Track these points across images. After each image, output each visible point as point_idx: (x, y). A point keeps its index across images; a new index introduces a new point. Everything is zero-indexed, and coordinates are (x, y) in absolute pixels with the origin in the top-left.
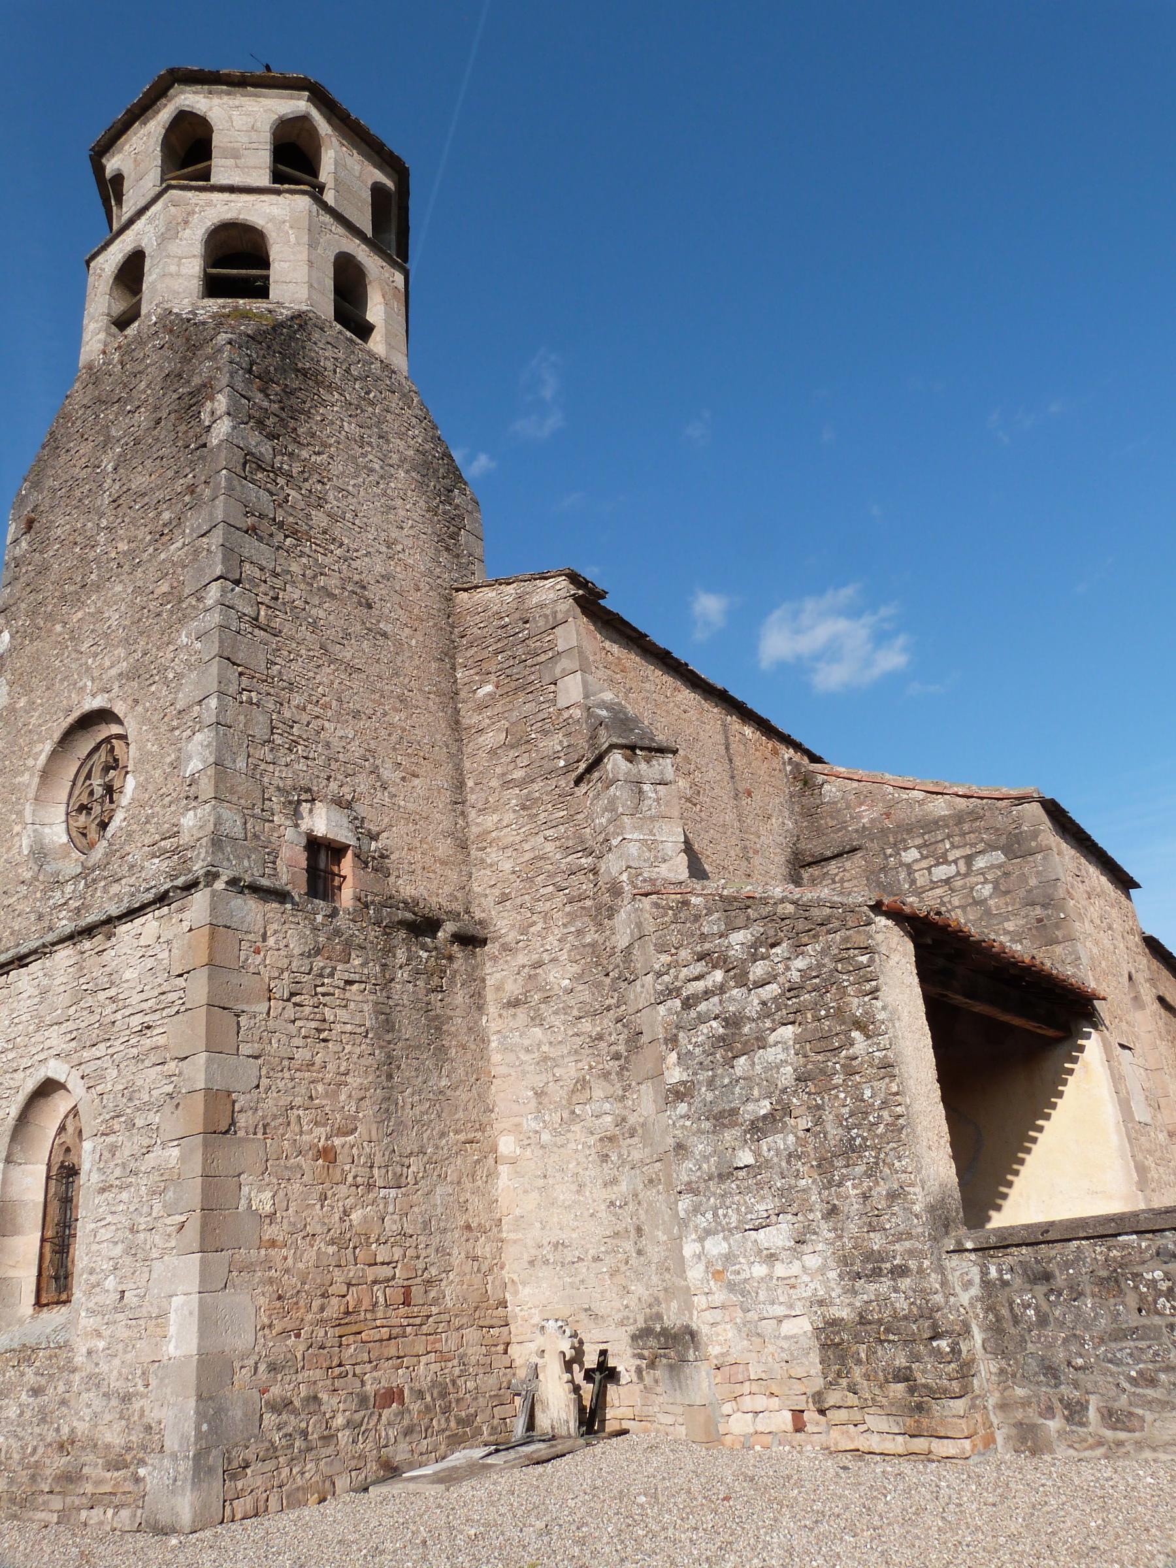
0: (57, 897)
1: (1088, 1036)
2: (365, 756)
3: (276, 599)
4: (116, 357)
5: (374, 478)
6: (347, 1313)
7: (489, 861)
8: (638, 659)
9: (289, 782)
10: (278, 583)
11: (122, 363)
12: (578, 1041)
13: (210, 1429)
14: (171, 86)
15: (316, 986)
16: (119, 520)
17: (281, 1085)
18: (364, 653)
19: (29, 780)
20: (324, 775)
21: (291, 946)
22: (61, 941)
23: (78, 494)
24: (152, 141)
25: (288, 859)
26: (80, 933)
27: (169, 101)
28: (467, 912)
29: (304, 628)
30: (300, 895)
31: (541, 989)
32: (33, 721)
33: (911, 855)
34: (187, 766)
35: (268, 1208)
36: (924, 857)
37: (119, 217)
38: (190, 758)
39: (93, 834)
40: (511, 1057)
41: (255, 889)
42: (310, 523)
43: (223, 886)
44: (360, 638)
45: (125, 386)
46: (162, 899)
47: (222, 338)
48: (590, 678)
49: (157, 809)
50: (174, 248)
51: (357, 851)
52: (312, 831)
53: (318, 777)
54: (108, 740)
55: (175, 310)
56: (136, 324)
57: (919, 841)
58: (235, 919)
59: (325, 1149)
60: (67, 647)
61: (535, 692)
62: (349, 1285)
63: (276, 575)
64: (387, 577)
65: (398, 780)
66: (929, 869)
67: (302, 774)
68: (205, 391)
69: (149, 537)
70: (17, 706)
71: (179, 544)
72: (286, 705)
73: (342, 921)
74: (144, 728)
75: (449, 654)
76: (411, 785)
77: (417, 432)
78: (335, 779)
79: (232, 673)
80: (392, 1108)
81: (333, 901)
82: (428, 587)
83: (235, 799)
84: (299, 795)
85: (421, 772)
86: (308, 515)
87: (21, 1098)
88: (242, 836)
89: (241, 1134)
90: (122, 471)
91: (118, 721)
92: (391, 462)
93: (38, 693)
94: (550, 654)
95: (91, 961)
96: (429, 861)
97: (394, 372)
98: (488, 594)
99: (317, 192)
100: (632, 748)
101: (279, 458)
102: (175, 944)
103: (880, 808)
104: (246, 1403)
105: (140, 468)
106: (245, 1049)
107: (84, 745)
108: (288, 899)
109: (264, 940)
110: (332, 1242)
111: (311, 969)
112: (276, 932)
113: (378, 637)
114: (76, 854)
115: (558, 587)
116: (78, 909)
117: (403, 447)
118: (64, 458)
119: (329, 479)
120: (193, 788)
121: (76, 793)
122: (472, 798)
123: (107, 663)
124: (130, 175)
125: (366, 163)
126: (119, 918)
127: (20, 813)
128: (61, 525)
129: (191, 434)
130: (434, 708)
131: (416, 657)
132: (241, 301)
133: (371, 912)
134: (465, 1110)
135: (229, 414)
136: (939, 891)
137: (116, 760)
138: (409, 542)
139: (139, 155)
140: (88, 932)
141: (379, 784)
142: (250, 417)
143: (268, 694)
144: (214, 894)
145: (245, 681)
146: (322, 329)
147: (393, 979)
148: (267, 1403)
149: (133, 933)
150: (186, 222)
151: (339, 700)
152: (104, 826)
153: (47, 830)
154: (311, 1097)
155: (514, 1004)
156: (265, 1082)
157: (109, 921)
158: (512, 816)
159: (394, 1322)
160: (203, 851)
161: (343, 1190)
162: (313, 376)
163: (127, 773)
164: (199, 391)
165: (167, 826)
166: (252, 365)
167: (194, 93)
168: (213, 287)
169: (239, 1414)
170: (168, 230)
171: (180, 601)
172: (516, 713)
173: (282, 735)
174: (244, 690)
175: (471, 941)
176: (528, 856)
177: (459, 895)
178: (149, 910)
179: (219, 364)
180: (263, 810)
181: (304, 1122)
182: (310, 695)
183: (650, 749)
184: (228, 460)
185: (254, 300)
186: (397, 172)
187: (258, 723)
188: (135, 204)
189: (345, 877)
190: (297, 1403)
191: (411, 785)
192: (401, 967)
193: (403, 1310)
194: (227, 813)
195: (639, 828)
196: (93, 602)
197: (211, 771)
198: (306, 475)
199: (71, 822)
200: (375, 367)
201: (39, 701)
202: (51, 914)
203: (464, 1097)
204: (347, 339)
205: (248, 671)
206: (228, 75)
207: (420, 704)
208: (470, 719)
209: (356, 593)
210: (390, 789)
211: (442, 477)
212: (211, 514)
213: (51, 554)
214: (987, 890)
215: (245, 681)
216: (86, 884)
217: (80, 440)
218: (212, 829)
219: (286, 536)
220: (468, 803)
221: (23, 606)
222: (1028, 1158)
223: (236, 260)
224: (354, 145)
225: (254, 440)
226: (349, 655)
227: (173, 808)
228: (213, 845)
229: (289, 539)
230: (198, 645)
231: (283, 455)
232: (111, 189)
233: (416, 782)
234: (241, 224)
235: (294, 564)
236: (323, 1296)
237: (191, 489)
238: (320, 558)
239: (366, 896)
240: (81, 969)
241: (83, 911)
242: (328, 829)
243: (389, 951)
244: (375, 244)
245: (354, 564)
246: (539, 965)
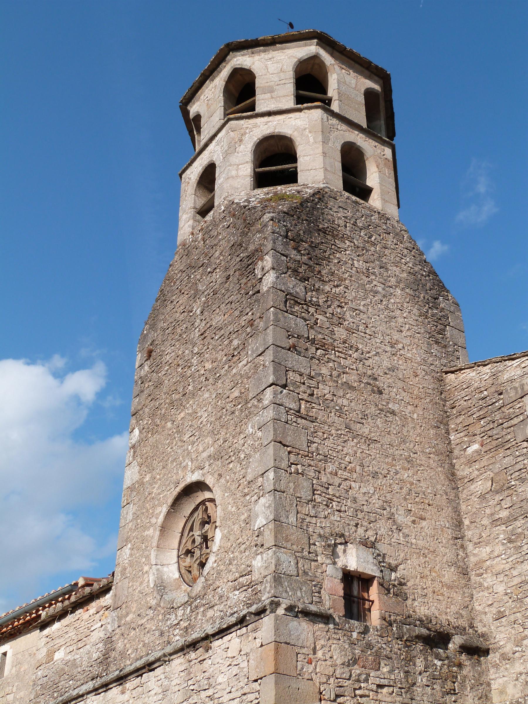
0: (173, 619)
2: (383, 506)
3: (312, 395)
4: (200, 236)
5: (378, 297)
7: (486, 585)
9: (328, 530)
10: (313, 383)
11: (204, 240)
14: (228, 54)
15: (355, 689)
16: (206, 347)
18: (378, 428)
19: (153, 533)
20: (353, 523)
21: (335, 657)
22: (176, 652)
23: (179, 331)
24: (218, 91)
25: (329, 590)
26: (188, 646)
27: (227, 64)
28: (472, 626)
29: (333, 414)
30: (339, 617)
32: (155, 491)
34: (255, 522)
37: (199, 141)
38: (257, 516)
39: (195, 572)
41: (306, 614)
42: (334, 337)
43: (283, 612)
44: (374, 417)
45: (206, 255)
46: (242, 622)
47: (267, 217)
49: (236, 554)
50: (234, 159)
51: (381, 581)
52: (346, 566)
53: (349, 525)
54: (203, 503)
55: (236, 201)
56: (212, 213)
58: (293, 637)
60: (175, 438)
61: (512, 449)
63: (311, 378)
64: (392, 369)
65: (410, 523)
67: (336, 524)
68: (257, 255)
69: (225, 358)
70: (145, 480)
71: (244, 362)
72: (323, 472)
73: (372, 637)
74: (226, 494)
75: (443, 422)
76: (420, 526)
77: (408, 259)
78: (362, 526)
79: (283, 452)
81: (365, 621)
82: (424, 373)
83: (289, 545)
84: (335, 540)
85: (427, 515)
86: (332, 332)
88: (295, 573)
90: (206, 313)
91: (209, 489)
92: (390, 284)
93: (158, 471)
94: (521, 418)
95: (196, 668)
96: (437, 586)
97: (388, 219)
98: (470, 374)
99: (326, 103)
101: (309, 294)
102: (251, 657)
105: (217, 311)
107: (188, 507)
108: (331, 621)
109: (315, 653)
111: (351, 676)
112: (323, 647)
113: (388, 415)
114: (184, 587)
115: (523, 365)
116: (186, 628)
117: (398, 272)
118: (170, 306)
119: (346, 304)
120: (260, 538)
121: (184, 541)
122: (469, 534)
123: (201, 449)
124: (204, 114)
125: (359, 77)
126: (214, 635)
127: (148, 557)
128: (169, 353)
129: (249, 284)
130: (434, 465)
131: (418, 427)
132: (279, 188)
133: (395, 629)
135: (273, 269)
137: (209, 517)
138: (407, 341)
139: (209, 103)
140: (193, 645)
141: (395, 527)
142: (288, 268)
143: (310, 465)
144: (277, 618)
145: (293, 458)
146: (335, 198)
147: (415, 684)
149: (223, 647)
150: (241, 141)
151: (362, 465)
152: (202, 565)
153: (165, 569)
157: (207, 637)
158: (501, 548)
160: (268, 585)
162: (330, 232)
163: (216, 527)
164: (253, 254)
165: (243, 566)
166: (287, 232)
167: (243, 55)
168: (261, 180)
170: (229, 148)
171: (247, 403)
172: (498, 465)
173: (321, 496)
174: (292, 464)
175: (476, 651)
176: (516, 581)
177: (463, 613)
178: (233, 630)
179: (266, 236)
180: (309, 553)
182: (340, 463)
184: (274, 301)
185: (288, 186)
186: (381, 78)
187: (303, 487)
188: (208, 133)
189: (373, 602)
191: (420, 526)
192: (420, 674)
196: (191, 405)
197: (271, 526)
198: (329, 303)
199: (181, 563)
200: (375, 218)
201: (158, 477)
202: (169, 632)
204: (353, 202)
205: (294, 450)
206: (264, 40)
207: (423, 462)
208: (463, 471)
209: (370, 384)
210: (404, 531)
211: (430, 288)
212: (264, 339)
213: (163, 373)
215: (293, 458)
216: (191, 610)
217: (179, 294)
218: (274, 568)
219: (317, 349)
220: (466, 538)
221: (147, 410)
223: (275, 161)
224: (351, 67)
225: (292, 284)
226: (367, 431)
227: (247, 553)
228: (275, 581)
229: (319, 351)
230: (260, 434)
231: (312, 291)
232: (194, 124)
233: (424, 523)
234: (277, 135)
235: (324, 368)
237: (251, 323)
238: (342, 361)
239: (390, 616)
240: (189, 673)
241: (190, 630)
242: (358, 564)
243: (410, 660)
244: (370, 132)
245: (367, 363)
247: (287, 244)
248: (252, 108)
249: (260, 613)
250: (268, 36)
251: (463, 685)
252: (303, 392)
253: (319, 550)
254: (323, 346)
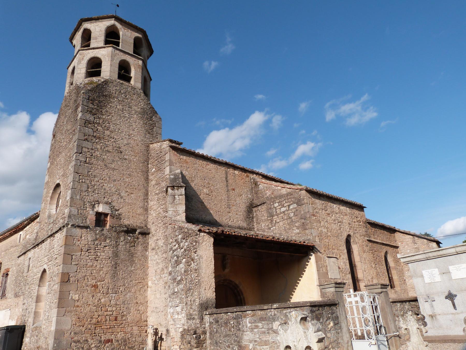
1: (312, 255)
6: (98, 322)
8: (193, 159)
9: (92, 200)
10: (93, 151)
12: (163, 259)
13: (57, 345)
17: (83, 271)
28: (146, 226)
31: (158, 246)
33: (276, 205)
35: (77, 298)
36: (279, 205)
40: (152, 262)
41: (79, 226)
48: (173, 167)
50: (80, 67)
57: (278, 201)
59: (95, 285)
62: (99, 316)
63: (92, 149)
66: (280, 209)
73: (105, 232)
79: (77, 176)
80: (116, 275)
87: (41, 272)
89: (71, 282)
96: (134, 215)
100: (173, 187)
103: (271, 192)
104: (67, 341)
106: (73, 263)
110: (95, 306)
134: (139, 275)
136: (282, 215)
148: (73, 341)
150: (83, 59)
153: (52, 211)
154: (92, 273)
155: (153, 249)
156: (78, 270)
159: (111, 324)
161: (99, 294)
169: (65, 343)
176: (158, 212)
177: (143, 222)
181: (89, 279)
183: (178, 187)
190: (81, 341)
193: (114, 322)
194: (73, 209)
195: (173, 207)
203: (139, 272)
208: (151, 177)
214: (292, 215)
222: (297, 288)
223: (94, 66)
233: (132, 195)
236: (91, 318)
246: (157, 240)
247: (88, 102)
248: (89, 46)
249: (64, 227)
250: (96, 16)
251: (138, 244)
252: (88, 155)
253: (88, 206)
254: (99, 138)
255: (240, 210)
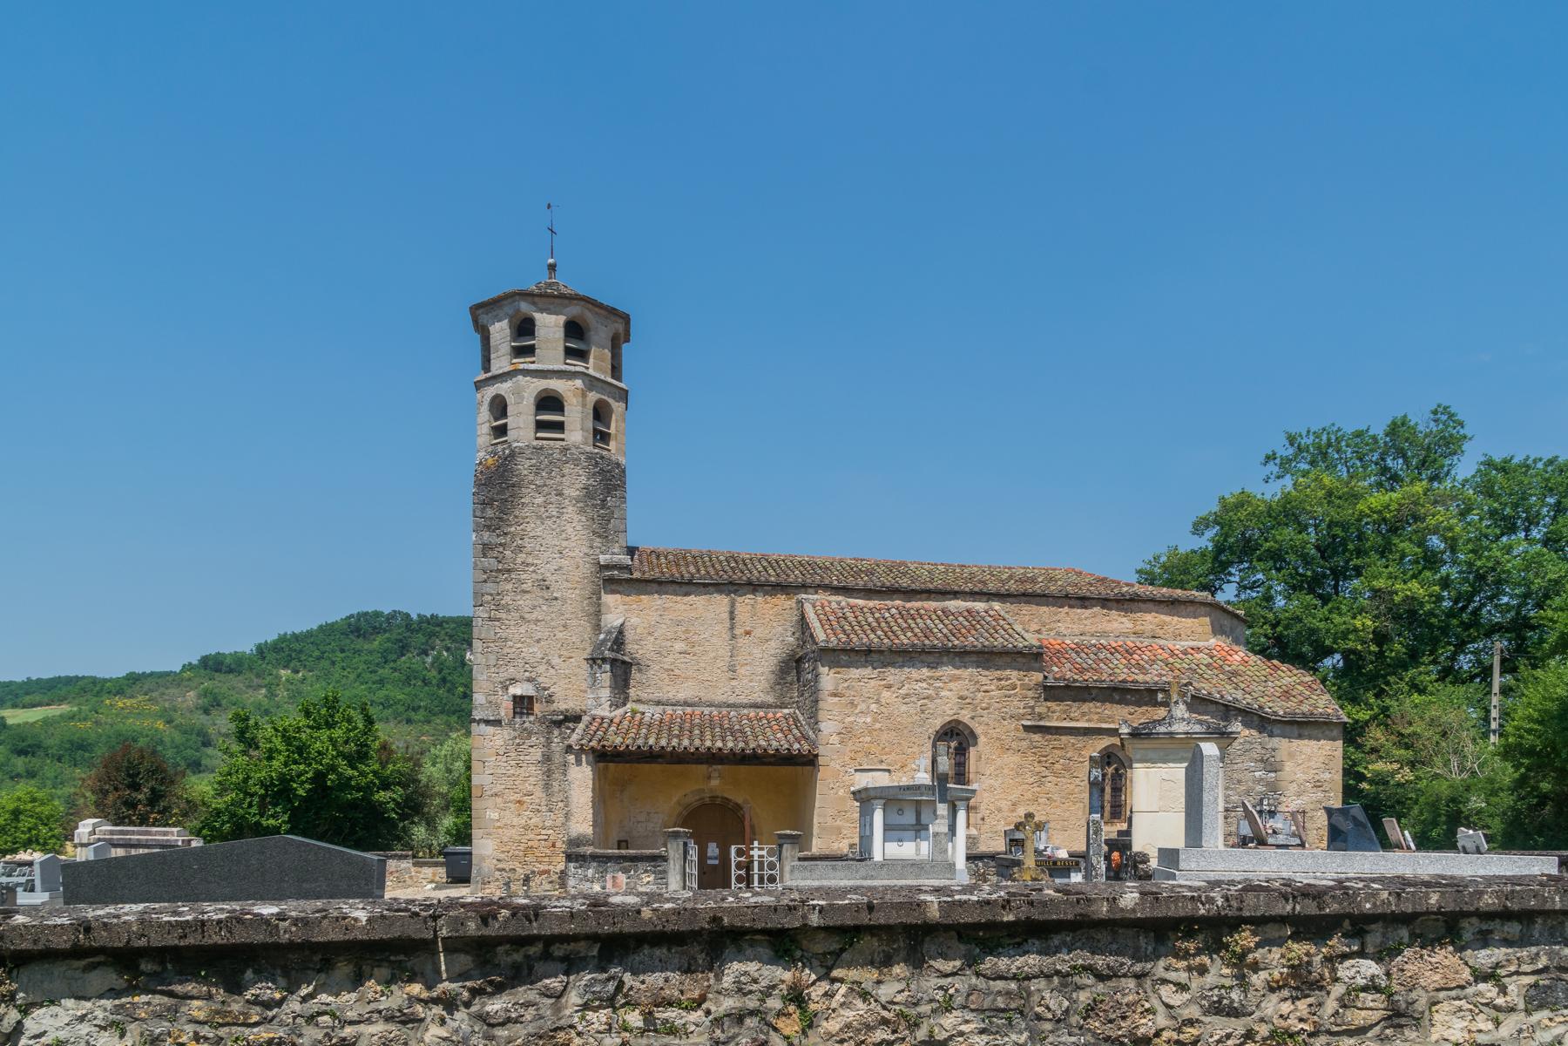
255: (760, 670)
